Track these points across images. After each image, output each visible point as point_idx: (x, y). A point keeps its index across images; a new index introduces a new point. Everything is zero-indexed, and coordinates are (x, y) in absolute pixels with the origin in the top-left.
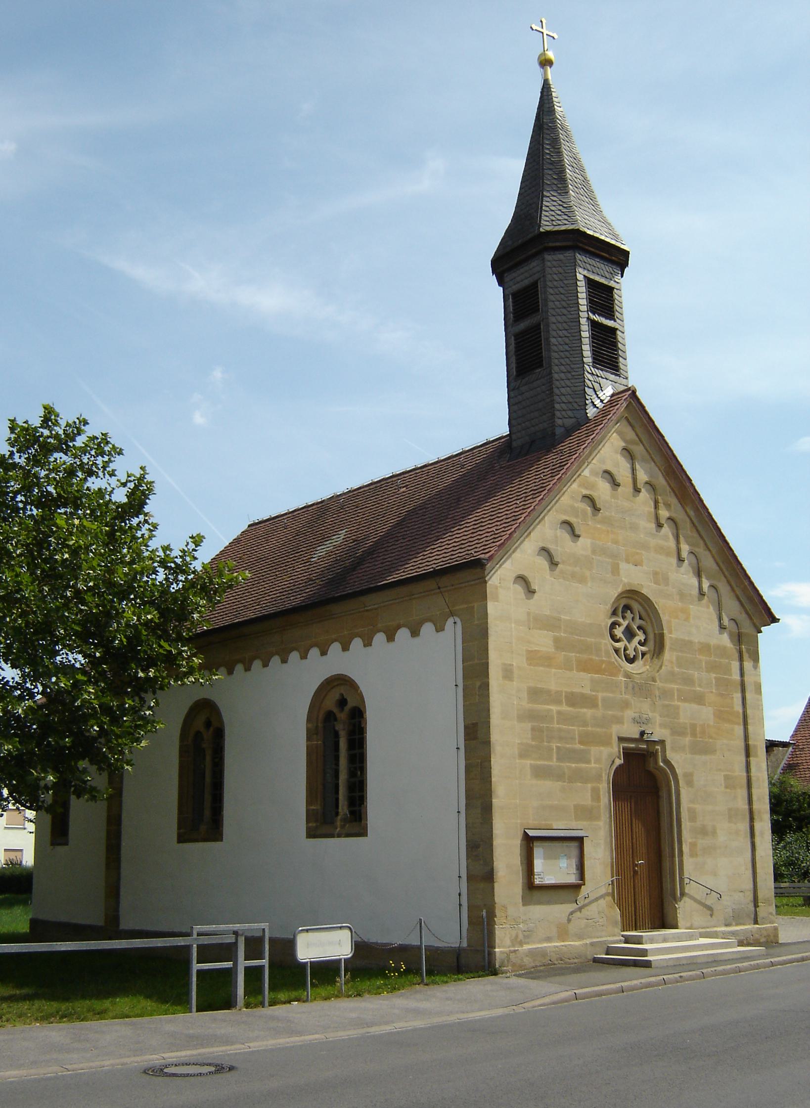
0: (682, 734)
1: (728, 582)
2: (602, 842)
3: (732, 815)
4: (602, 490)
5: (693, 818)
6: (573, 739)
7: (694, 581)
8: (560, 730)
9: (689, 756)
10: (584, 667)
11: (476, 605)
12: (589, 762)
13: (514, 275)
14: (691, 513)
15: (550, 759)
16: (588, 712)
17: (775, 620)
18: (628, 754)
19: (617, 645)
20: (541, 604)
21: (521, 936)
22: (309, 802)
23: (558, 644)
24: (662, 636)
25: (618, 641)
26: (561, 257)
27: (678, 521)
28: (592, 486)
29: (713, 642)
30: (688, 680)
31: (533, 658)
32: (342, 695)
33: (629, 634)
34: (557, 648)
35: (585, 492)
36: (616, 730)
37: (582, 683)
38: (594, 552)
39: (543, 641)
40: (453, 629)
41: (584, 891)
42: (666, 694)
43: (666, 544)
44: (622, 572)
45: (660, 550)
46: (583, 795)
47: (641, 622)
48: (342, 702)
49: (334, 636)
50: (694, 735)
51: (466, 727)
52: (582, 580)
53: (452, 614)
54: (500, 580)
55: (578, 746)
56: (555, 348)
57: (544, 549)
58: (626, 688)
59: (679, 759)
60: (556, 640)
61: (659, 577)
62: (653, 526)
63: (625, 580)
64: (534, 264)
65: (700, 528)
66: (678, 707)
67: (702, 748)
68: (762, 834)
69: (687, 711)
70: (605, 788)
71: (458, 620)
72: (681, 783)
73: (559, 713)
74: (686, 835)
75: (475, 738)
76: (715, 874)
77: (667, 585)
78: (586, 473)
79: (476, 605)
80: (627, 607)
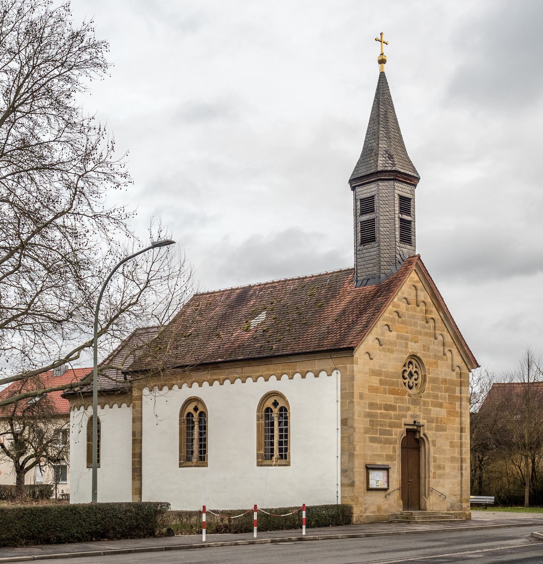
0: (432, 422)
1: (457, 348)
2: (396, 470)
3: (453, 459)
4: (403, 306)
5: (435, 461)
6: (386, 425)
7: (441, 349)
8: (380, 421)
9: (434, 432)
10: (392, 392)
11: (348, 366)
12: (392, 435)
13: (362, 189)
14: (442, 315)
15: (376, 434)
16: (392, 413)
17: (478, 366)
18: (408, 431)
19: (405, 381)
20: (375, 365)
21: (363, 510)
22: (258, 449)
23: (381, 382)
24: (425, 376)
25: (405, 379)
26: (387, 184)
27: (435, 319)
28: (398, 306)
29: (448, 378)
30: (436, 397)
31: (372, 389)
32: (275, 400)
33: (411, 375)
34: (381, 384)
35: (395, 309)
36: (403, 420)
37: (391, 399)
38: (397, 338)
39: (375, 381)
40: (336, 376)
41: (389, 491)
42: (425, 404)
43: (429, 331)
44: (409, 346)
45: (426, 334)
46: (389, 450)
47: (416, 369)
48: (275, 404)
49: (272, 373)
50: (437, 422)
51: (341, 420)
52: (392, 351)
53: (336, 369)
54: (359, 353)
55: (388, 428)
56: (382, 233)
57: (377, 339)
58: (409, 401)
59: (429, 432)
60: (380, 380)
61: (426, 348)
62: (424, 322)
63: (410, 351)
64: (373, 186)
65: (445, 322)
66: (431, 410)
67: (440, 429)
68: (466, 469)
69: (435, 412)
70: (398, 446)
71: (338, 371)
72: (431, 444)
73: (381, 413)
74: (432, 469)
75: (346, 425)
76: (443, 486)
77: (429, 351)
78: (396, 300)
79: (348, 366)
80: (410, 363)
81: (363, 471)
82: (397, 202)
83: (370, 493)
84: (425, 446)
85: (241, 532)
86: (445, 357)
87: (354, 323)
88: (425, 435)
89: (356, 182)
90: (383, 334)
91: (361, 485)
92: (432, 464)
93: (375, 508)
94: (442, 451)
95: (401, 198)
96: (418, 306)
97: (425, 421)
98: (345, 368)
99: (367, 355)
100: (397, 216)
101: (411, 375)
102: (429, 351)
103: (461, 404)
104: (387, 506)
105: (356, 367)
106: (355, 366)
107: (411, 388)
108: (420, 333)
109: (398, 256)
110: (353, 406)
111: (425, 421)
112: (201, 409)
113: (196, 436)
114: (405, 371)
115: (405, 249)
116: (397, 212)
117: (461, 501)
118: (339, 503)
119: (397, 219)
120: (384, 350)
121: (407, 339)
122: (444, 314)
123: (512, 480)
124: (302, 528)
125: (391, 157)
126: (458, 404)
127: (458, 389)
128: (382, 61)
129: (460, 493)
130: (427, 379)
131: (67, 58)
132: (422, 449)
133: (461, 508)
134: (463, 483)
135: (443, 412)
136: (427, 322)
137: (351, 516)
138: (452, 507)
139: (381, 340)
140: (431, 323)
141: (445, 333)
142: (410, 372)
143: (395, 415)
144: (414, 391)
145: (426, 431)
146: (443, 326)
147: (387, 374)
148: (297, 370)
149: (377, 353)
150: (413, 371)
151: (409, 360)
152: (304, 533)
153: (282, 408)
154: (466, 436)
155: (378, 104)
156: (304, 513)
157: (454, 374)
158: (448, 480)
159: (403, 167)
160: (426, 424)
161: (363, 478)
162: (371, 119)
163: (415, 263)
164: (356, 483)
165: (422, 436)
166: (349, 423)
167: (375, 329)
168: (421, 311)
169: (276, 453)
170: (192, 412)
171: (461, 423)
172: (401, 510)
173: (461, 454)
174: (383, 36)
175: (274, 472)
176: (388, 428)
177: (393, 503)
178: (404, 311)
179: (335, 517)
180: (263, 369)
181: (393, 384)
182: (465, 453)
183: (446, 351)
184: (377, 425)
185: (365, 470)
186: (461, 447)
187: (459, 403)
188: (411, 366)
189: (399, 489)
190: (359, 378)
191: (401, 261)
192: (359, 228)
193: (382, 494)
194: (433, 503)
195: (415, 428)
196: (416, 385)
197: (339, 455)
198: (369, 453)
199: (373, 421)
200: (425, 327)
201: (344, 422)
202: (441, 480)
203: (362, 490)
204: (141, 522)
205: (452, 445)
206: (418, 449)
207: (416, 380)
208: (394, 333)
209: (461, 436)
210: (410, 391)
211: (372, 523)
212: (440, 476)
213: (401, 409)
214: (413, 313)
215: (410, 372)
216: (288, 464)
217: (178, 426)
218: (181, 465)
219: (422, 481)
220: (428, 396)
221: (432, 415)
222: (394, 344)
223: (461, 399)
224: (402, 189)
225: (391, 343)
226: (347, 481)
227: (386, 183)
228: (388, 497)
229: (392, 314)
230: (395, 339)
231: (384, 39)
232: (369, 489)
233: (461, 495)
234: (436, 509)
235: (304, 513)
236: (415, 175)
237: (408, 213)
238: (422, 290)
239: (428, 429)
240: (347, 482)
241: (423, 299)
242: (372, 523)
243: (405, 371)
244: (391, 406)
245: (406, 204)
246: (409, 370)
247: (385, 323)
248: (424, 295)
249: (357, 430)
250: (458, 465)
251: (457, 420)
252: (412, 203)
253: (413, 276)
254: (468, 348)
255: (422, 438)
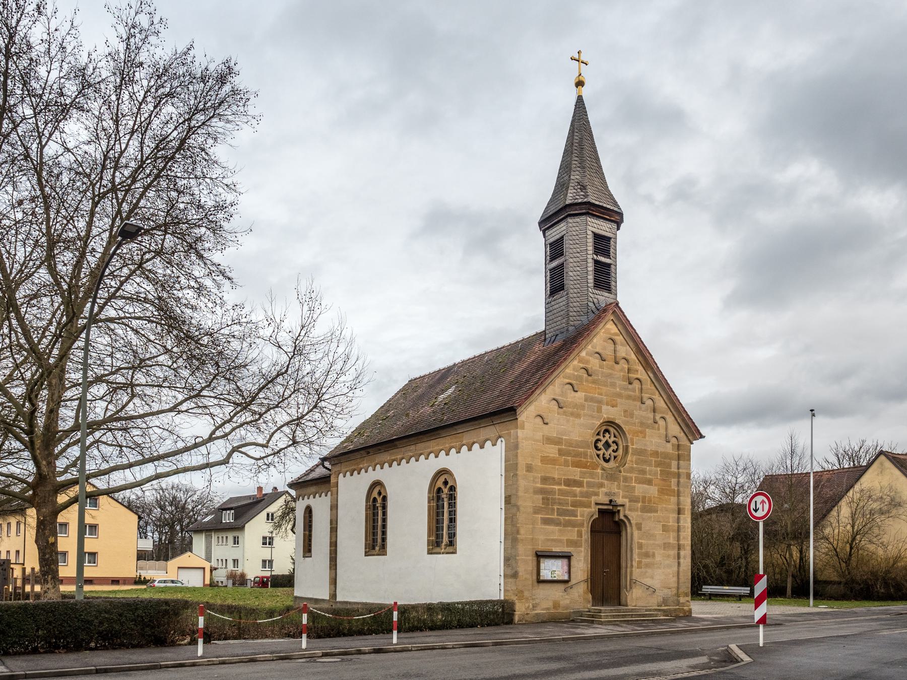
0: (637, 501)
3: (666, 546)
7: (651, 415)
10: (576, 465)
12: (576, 516)
14: (651, 375)
16: (578, 490)
17: (702, 437)
18: (600, 511)
19: (598, 452)
20: (552, 430)
21: (531, 607)
22: (429, 536)
24: (627, 447)
26: (578, 220)
28: (587, 362)
30: (643, 472)
31: (545, 460)
34: (560, 454)
35: (582, 365)
36: (594, 499)
37: (575, 473)
38: (586, 400)
39: (552, 451)
40: (501, 445)
42: (626, 479)
45: (629, 397)
50: (643, 502)
52: (578, 416)
53: (500, 437)
54: (527, 415)
55: (570, 508)
57: (554, 399)
59: (632, 514)
60: (559, 450)
61: (628, 413)
68: (685, 558)
69: (640, 489)
72: (634, 528)
74: (635, 557)
76: (652, 578)
78: (583, 354)
80: (607, 431)
81: (531, 559)
82: (590, 240)
83: (542, 586)
84: (626, 530)
85: (328, 636)
86: (657, 426)
87: (527, 381)
88: (626, 516)
89: (547, 222)
90: (563, 394)
91: (528, 576)
92: (636, 551)
93: (550, 604)
94: (651, 536)
95: (596, 236)
96: (617, 363)
97: (627, 500)
98: (509, 434)
99: (539, 420)
100: (590, 257)
101: (607, 445)
102: (632, 417)
103: (679, 482)
104: (568, 602)
105: (520, 432)
106: (519, 431)
107: (607, 461)
108: (619, 395)
109: (591, 304)
110: (517, 480)
111: (627, 500)
112: (383, 494)
113: (380, 523)
114: (599, 440)
115: (603, 297)
116: (591, 252)
117: (678, 595)
118: (502, 598)
119: (590, 261)
120: (565, 413)
121: (600, 402)
122: (655, 374)
123: (777, 570)
124: (197, 643)
125: (583, 188)
126: (674, 481)
127: (674, 463)
128: (580, 84)
129: (676, 585)
130: (630, 450)
131: (205, 103)
132: (623, 534)
133: (678, 603)
134: (681, 574)
135: (653, 491)
136: (630, 383)
137: (513, 615)
138: (665, 601)
139: (560, 401)
140: (636, 385)
141: (657, 397)
142: (607, 442)
143: (581, 492)
144: (612, 464)
145: (627, 513)
146: (654, 388)
147: (570, 443)
148: (464, 442)
149: (551, 417)
150: (610, 441)
151: (604, 428)
152: (395, 641)
153: (451, 486)
154: (685, 518)
155: (573, 132)
156: (395, 613)
157: (669, 445)
158: (658, 569)
159: (598, 199)
160: (627, 505)
161: (531, 565)
162: (566, 151)
163: (615, 310)
164: (520, 574)
165: (622, 517)
166: (513, 501)
167: (551, 387)
168: (622, 370)
169: (445, 539)
170: (377, 496)
171: (678, 504)
172: (589, 606)
173: (678, 540)
174: (582, 55)
175: (442, 560)
176: (570, 508)
177: (578, 597)
178: (596, 367)
179: (493, 616)
180: (433, 444)
181: (578, 455)
182: (684, 538)
183: (657, 418)
184: (553, 504)
185: (535, 558)
186: (678, 531)
187: (676, 480)
188: (607, 435)
189: (586, 581)
190: (525, 447)
191: (594, 310)
192: (548, 278)
193: (562, 587)
194: (635, 599)
195: (611, 507)
196: (615, 457)
197: (503, 540)
198: (542, 537)
199: (548, 499)
200: (626, 389)
201: (508, 500)
202: (649, 570)
203: (530, 582)
204: (150, 623)
205: (665, 529)
206: (619, 533)
207: (613, 451)
208: (580, 395)
209: (678, 519)
210: (605, 465)
211: (543, 622)
212: (648, 566)
213: (589, 485)
214: (610, 371)
215: (607, 442)
216: (454, 552)
217: (364, 512)
218: (367, 554)
219: (623, 571)
220: (631, 470)
221: (637, 493)
222: (582, 407)
223: (678, 475)
224: (603, 227)
225: (575, 406)
226: (510, 572)
227: (577, 219)
228: (569, 590)
229: (577, 371)
230: (582, 401)
231: (582, 58)
232: (540, 581)
233: (678, 588)
234: (641, 604)
235: (395, 613)
236: (616, 209)
237: (607, 254)
238: (622, 345)
239: (630, 510)
240: (511, 574)
241: (624, 355)
242: (543, 622)
243: (598, 440)
244: (575, 481)
245: (603, 244)
246: (604, 440)
247: (568, 381)
248: (625, 351)
249: (522, 509)
250: (673, 552)
251: (674, 499)
252: (612, 243)
253: (609, 327)
254: (688, 415)
255: (622, 520)
